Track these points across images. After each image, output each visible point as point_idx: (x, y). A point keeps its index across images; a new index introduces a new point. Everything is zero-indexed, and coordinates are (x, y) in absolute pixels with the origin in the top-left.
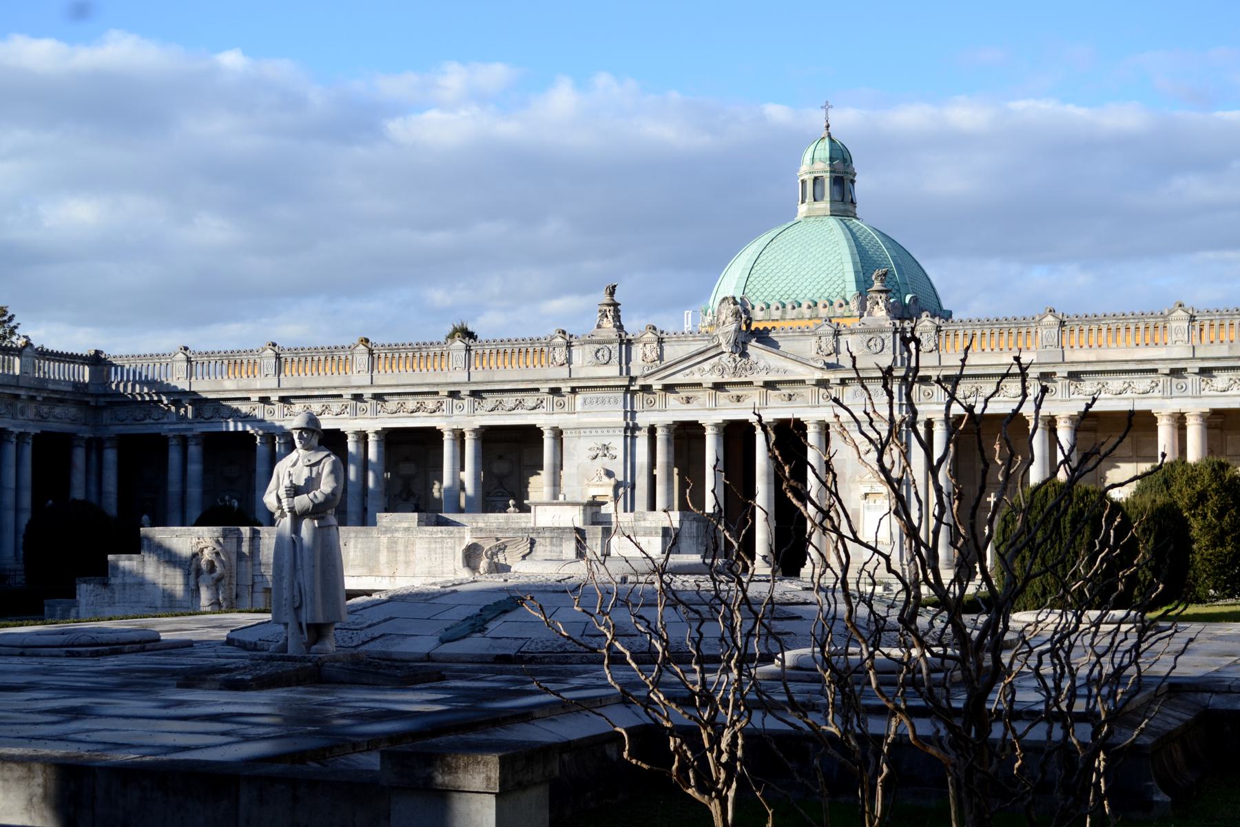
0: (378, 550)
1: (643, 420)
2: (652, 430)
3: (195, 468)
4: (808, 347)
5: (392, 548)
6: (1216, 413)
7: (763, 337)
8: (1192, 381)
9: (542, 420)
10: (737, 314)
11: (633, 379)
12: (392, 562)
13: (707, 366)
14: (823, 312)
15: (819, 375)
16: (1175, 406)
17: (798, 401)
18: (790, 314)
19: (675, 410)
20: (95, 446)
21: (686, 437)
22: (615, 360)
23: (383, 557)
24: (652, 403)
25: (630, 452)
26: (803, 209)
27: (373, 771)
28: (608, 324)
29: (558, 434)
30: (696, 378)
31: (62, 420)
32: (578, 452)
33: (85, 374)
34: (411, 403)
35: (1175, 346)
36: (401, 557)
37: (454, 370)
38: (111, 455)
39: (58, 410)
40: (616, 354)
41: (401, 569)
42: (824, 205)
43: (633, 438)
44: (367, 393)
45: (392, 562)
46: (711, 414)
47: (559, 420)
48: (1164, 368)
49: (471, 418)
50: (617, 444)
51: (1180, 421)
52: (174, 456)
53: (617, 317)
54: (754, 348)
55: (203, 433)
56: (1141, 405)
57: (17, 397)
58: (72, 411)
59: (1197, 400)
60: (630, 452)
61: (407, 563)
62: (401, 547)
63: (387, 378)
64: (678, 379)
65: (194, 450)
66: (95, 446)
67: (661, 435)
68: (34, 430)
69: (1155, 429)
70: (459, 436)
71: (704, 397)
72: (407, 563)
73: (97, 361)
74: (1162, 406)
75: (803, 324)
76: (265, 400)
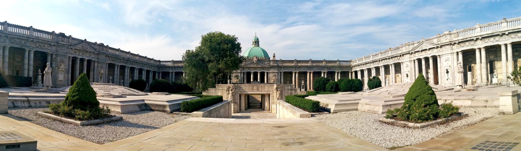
3: (174, 76)
5: (261, 88)
19: (247, 70)
20: (159, 73)
23: (260, 89)
38: (161, 74)
52: (171, 75)
55: (486, 47)
66: (159, 73)
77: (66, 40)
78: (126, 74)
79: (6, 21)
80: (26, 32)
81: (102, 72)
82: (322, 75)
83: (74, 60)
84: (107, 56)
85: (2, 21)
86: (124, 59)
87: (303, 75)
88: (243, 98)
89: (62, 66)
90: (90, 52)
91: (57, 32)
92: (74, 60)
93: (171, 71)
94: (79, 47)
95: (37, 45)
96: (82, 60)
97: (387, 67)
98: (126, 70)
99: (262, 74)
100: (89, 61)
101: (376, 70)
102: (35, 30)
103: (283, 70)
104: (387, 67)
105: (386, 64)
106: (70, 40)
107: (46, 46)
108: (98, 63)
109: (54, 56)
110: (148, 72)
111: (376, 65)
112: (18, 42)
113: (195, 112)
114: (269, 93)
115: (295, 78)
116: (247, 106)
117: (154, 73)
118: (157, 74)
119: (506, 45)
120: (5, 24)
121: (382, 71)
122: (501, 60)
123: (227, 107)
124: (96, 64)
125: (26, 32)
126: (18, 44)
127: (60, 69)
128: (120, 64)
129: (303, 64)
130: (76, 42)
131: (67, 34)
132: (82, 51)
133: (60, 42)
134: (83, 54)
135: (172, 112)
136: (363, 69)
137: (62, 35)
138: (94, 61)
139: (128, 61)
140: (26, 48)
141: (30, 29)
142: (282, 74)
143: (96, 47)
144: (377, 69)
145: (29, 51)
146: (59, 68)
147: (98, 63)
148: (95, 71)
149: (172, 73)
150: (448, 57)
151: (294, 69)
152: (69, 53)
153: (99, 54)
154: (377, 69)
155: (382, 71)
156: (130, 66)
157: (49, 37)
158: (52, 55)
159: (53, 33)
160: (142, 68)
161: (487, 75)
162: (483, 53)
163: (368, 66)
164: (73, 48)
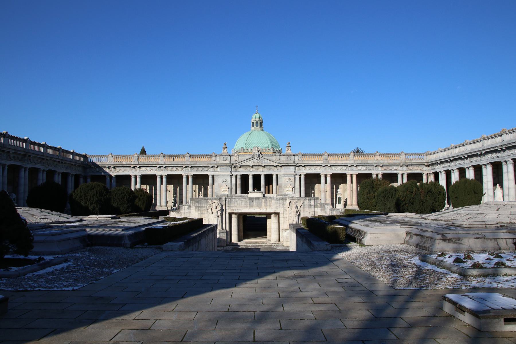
0: (262, 203)
1: (234, 173)
2: (236, 176)
6: (333, 174)
8: (163, 169)
9: (209, 172)
12: (266, 205)
13: (250, 162)
15: (277, 164)
16: (135, 174)
17: (247, 170)
19: (242, 171)
21: (245, 178)
22: (228, 160)
23: (263, 204)
24: (214, 170)
25: (231, 181)
26: (253, 128)
27: (288, 252)
29: (213, 176)
30: (248, 164)
31: (79, 171)
32: (218, 181)
33: (82, 159)
34: (175, 169)
36: (268, 204)
37: (353, 159)
41: (268, 207)
42: (258, 128)
45: (266, 205)
46: (251, 172)
47: (213, 173)
49: (139, 173)
50: (292, 178)
56: (395, 172)
57: (72, 164)
60: (231, 181)
61: (270, 206)
62: (268, 202)
64: (244, 164)
67: (239, 177)
68: (75, 174)
69: (346, 177)
70: (161, 177)
72: (270, 206)
73: (85, 156)
75: (249, 153)
76: (109, 168)
78: (22, 181)
80: (57, 153)
82: (424, 181)
85: (4, 131)
88: (234, 219)
97: (497, 167)
98: (22, 174)
101: (475, 171)
102: (78, 155)
104: (497, 167)
105: (496, 160)
110: (65, 176)
111: (475, 161)
113: (169, 244)
114: (277, 211)
116: (242, 234)
117: (77, 178)
118: (81, 180)
120: (6, 136)
121: (488, 174)
122: (320, 183)
123: (210, 235)
125: (57, 153)
129: (72, 224)
135: (132, 246)
136: (450, 169)
139: (25, 155)
142: (303, 177)
144: (478, 169)
150: (290, 178)
154: (478, 169)
155: (488, 174)
156: (29, 166)
160: (53, 169)
161: (156, 194)
162: (329, 179)
163: (460, 164)
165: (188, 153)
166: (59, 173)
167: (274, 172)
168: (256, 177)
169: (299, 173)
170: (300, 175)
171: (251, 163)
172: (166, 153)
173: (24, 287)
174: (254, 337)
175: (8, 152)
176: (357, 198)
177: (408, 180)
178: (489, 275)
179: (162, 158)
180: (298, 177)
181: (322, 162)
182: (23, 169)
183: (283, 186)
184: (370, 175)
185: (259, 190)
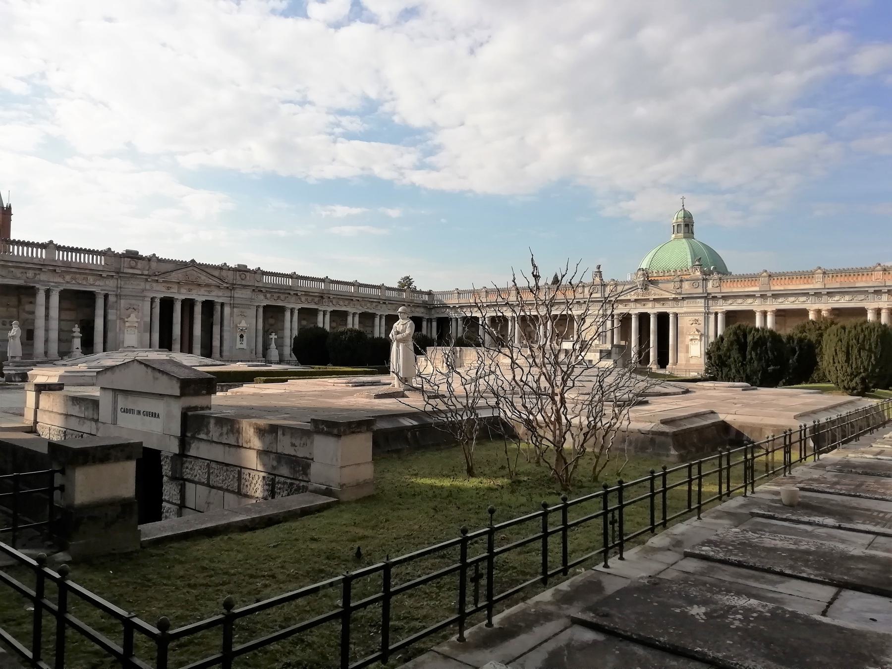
3: (54, 312)
4: (671, 286)
7: (654, 283)
10: (644, 274)
11: (709, 294)
14: (679, 273)
15: (674, 296)
18: (667, 274)
19: (621, 309)
20: (430, 321)
21: (626, 319)
28: (598, 279)
30: (629, 297)
33: (426, 298)
35: (817, 284)
38: (434, 324)
39: (418, 309)
40: (701, 284)
42: (681, 235)
43: (708, 318)
44: (769, 294)
46: (635, 310)
47: (676, 310)
48: (758, 294)
50: (701, 319)
51: (765, 314)
53: (601, 276)
54: (651, 287)
58: (422, 310)
59: (772, 306)
63: (777, 287)
64: (622, 298)
65: (460, 322)
66: (430, 321)
67: (720, 317)
71: (650, 305)
74: (756, 306)
77: (140, 264)
79: (109, 249)
80: (290, 282)
81: (243, 324)
82: (758, 324)
83: (167, 304)
84: (258, 290)
86: (307, 293)
87: (802, 440)
89: (133, 318)
90: (208, 285)
91: (119, 249)
92: (167, 304)
93: (453, 314)
94: (174, 277)
95: (68, 278)
96: (188, 305)
99: (663, 318)
100: (208, 306)
102: (59, 248)
103: (723, 307)
106: (154, 265)
107: (91, 279)
108: (233, 306)
109: (112, 299)
112: (19, 275)
115: (514, 330)
118: (424, 324)
119: (292, 310)
124: (227, 310)
125: (42, 254)
126: (18, 278)
127: (127, 324)
128: (300, 306)
130: (170, 267)
131: (144, 252)
132: (186, 284)
133: (126, 270)
134: (190, 290)
137: (132, 256)
138: (222, 305)
140: (37, 286)
141: (293, 276)
143: (224, 273)
145: (48, 293)
146: (125, 322)
147: (233, 306)
148: (226, 322)
149: (354, 314)
151: (758, 301)
152: (151, 290)
153: (232, 287)
157: (99, 261)
158: (106, 296)
159: (107, 253)
164: (161, 280)
165: (766, 271)
166: (381, 316)
167: (670, 309)
168: (644, 318)
169: (713, 309)
170: (716, 314)
171: (632, 296)
172: (828, 267)
173: (729, 515)
174: (566, 628)
175: (297, 295)
176: (658, 356)
177: (776, 322)
178: (311, 491)
179: (819, 276)
180: (712, 317)
181: (757, 289)
182: (322, 313)
183: (685, 331)
184: (804, 313)
185: (190, 351)
